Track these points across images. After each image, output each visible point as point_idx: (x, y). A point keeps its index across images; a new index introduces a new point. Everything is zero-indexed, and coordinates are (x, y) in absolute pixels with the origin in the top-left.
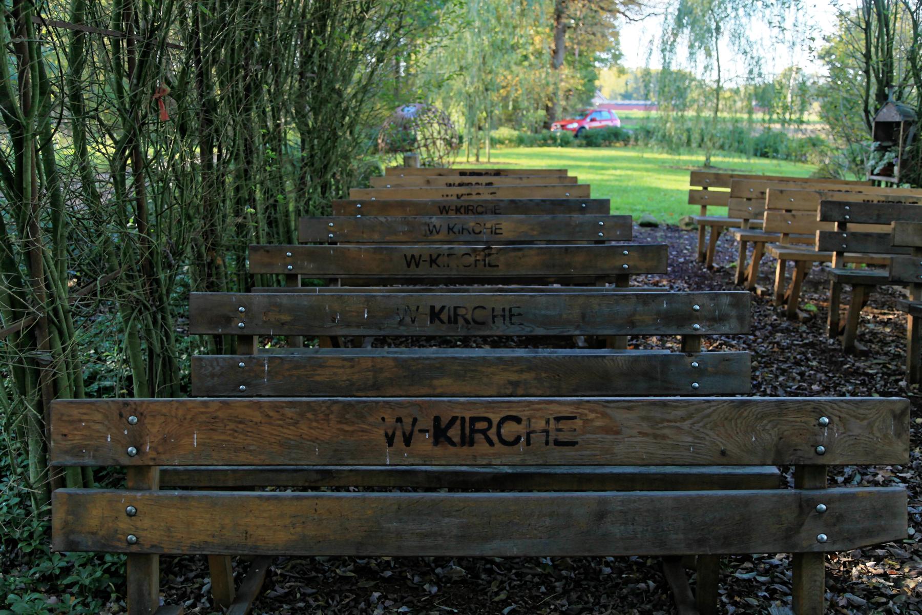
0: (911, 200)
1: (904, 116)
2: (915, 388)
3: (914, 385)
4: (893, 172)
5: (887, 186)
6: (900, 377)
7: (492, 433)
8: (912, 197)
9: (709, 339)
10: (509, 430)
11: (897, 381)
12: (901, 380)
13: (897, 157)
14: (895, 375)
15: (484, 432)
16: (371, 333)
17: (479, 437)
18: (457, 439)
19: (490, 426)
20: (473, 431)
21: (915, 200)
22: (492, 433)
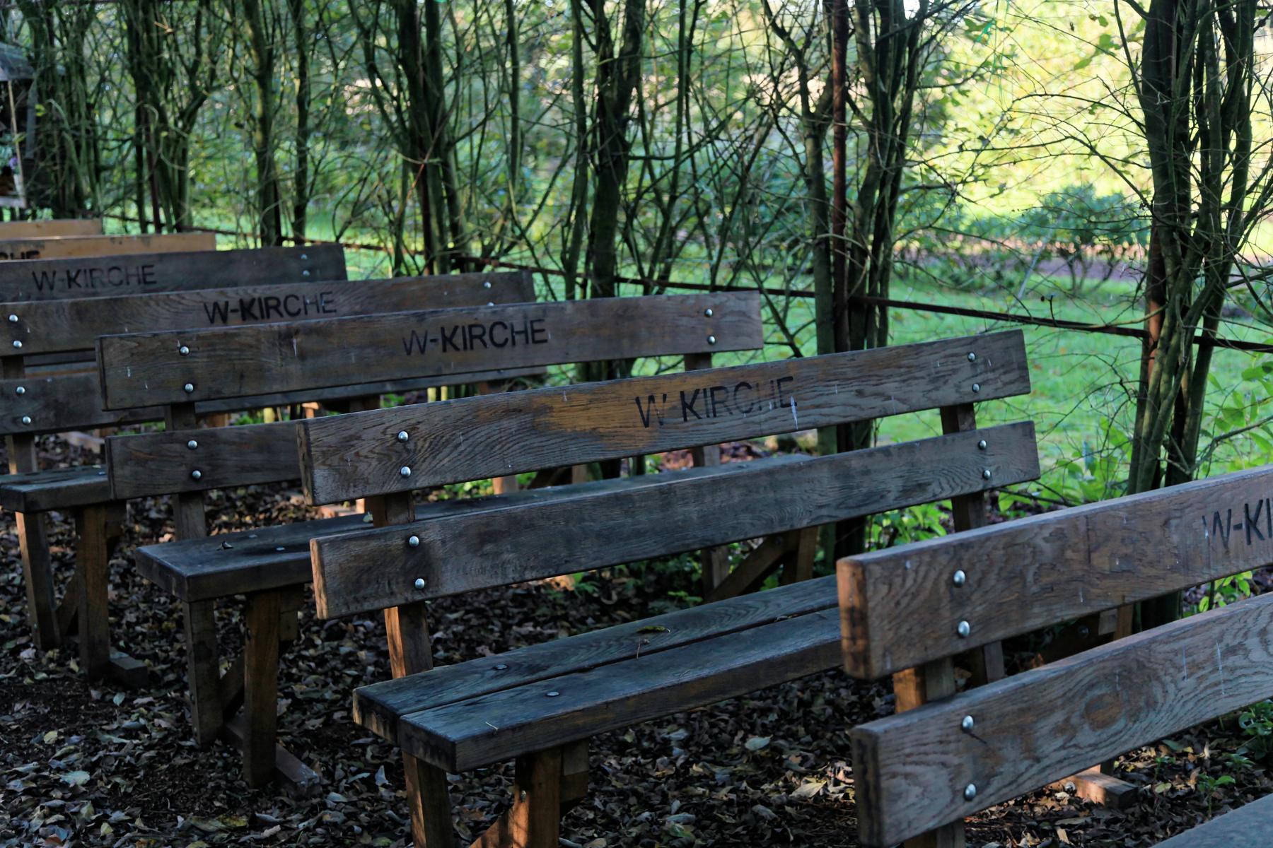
0: (24, 249)
1: (11, 70)
2: (51, 660)
3: (50, 653)
4: (12, 188)
5: (13, 218)
6: (23, 640)
7: (486, 338)
8: (25, 242)
9: (721, 187)
10: (500, 334)
11: (16, 651)
12: (26, 646)
13: (14, 154)
14: (14, 637)
15: (480, 337)
16: (638, 173)
17: (477, 342)
18: (461, 346)
19: (484, 333)
20: (472, 337)
21: (32, 248)
22: (486, 338)
